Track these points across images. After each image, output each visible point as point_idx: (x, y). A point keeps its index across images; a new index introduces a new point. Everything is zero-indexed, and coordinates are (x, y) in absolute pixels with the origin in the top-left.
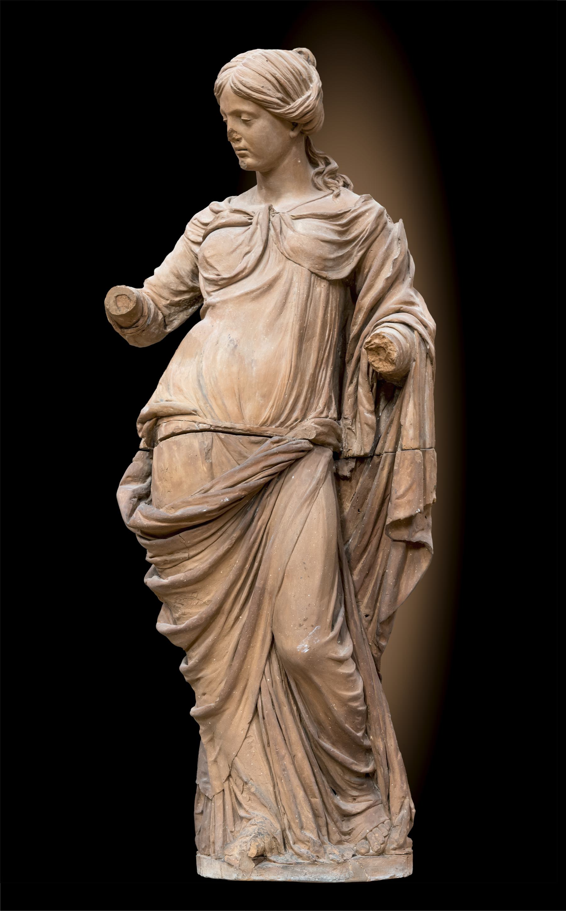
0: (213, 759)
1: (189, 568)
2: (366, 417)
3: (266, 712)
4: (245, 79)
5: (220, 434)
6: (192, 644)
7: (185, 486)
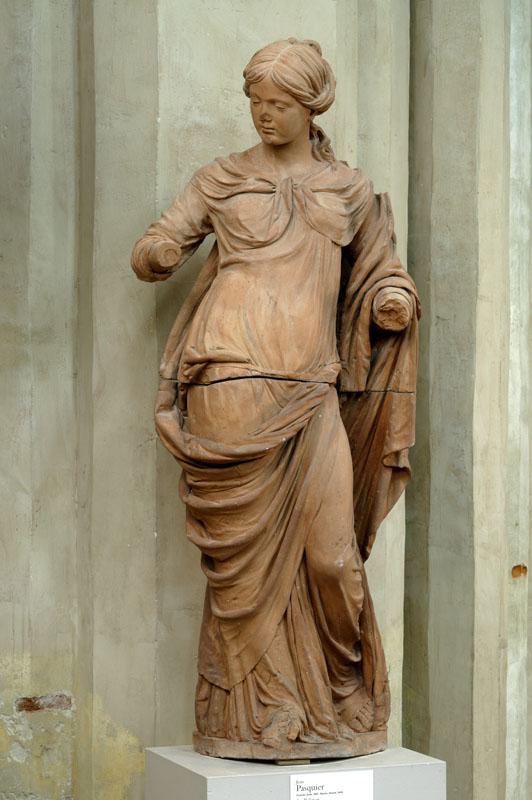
0: (236, 654)
1: (239, 494)
2: (364, 362)
3: (295, 615)
4: (287, 76)
5: (269, 380)
6: (229, 559)
7: (241, 425)
